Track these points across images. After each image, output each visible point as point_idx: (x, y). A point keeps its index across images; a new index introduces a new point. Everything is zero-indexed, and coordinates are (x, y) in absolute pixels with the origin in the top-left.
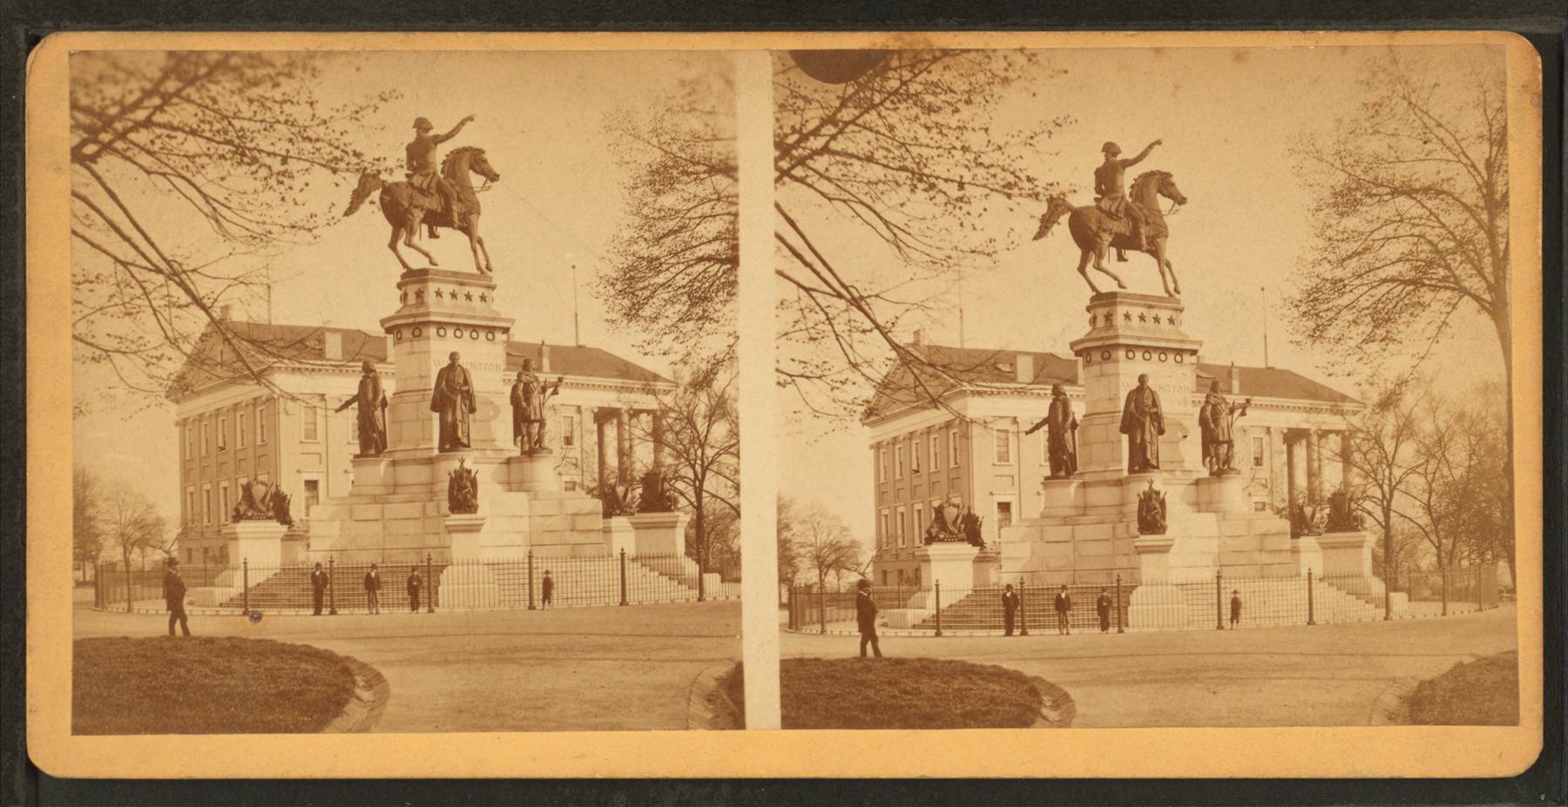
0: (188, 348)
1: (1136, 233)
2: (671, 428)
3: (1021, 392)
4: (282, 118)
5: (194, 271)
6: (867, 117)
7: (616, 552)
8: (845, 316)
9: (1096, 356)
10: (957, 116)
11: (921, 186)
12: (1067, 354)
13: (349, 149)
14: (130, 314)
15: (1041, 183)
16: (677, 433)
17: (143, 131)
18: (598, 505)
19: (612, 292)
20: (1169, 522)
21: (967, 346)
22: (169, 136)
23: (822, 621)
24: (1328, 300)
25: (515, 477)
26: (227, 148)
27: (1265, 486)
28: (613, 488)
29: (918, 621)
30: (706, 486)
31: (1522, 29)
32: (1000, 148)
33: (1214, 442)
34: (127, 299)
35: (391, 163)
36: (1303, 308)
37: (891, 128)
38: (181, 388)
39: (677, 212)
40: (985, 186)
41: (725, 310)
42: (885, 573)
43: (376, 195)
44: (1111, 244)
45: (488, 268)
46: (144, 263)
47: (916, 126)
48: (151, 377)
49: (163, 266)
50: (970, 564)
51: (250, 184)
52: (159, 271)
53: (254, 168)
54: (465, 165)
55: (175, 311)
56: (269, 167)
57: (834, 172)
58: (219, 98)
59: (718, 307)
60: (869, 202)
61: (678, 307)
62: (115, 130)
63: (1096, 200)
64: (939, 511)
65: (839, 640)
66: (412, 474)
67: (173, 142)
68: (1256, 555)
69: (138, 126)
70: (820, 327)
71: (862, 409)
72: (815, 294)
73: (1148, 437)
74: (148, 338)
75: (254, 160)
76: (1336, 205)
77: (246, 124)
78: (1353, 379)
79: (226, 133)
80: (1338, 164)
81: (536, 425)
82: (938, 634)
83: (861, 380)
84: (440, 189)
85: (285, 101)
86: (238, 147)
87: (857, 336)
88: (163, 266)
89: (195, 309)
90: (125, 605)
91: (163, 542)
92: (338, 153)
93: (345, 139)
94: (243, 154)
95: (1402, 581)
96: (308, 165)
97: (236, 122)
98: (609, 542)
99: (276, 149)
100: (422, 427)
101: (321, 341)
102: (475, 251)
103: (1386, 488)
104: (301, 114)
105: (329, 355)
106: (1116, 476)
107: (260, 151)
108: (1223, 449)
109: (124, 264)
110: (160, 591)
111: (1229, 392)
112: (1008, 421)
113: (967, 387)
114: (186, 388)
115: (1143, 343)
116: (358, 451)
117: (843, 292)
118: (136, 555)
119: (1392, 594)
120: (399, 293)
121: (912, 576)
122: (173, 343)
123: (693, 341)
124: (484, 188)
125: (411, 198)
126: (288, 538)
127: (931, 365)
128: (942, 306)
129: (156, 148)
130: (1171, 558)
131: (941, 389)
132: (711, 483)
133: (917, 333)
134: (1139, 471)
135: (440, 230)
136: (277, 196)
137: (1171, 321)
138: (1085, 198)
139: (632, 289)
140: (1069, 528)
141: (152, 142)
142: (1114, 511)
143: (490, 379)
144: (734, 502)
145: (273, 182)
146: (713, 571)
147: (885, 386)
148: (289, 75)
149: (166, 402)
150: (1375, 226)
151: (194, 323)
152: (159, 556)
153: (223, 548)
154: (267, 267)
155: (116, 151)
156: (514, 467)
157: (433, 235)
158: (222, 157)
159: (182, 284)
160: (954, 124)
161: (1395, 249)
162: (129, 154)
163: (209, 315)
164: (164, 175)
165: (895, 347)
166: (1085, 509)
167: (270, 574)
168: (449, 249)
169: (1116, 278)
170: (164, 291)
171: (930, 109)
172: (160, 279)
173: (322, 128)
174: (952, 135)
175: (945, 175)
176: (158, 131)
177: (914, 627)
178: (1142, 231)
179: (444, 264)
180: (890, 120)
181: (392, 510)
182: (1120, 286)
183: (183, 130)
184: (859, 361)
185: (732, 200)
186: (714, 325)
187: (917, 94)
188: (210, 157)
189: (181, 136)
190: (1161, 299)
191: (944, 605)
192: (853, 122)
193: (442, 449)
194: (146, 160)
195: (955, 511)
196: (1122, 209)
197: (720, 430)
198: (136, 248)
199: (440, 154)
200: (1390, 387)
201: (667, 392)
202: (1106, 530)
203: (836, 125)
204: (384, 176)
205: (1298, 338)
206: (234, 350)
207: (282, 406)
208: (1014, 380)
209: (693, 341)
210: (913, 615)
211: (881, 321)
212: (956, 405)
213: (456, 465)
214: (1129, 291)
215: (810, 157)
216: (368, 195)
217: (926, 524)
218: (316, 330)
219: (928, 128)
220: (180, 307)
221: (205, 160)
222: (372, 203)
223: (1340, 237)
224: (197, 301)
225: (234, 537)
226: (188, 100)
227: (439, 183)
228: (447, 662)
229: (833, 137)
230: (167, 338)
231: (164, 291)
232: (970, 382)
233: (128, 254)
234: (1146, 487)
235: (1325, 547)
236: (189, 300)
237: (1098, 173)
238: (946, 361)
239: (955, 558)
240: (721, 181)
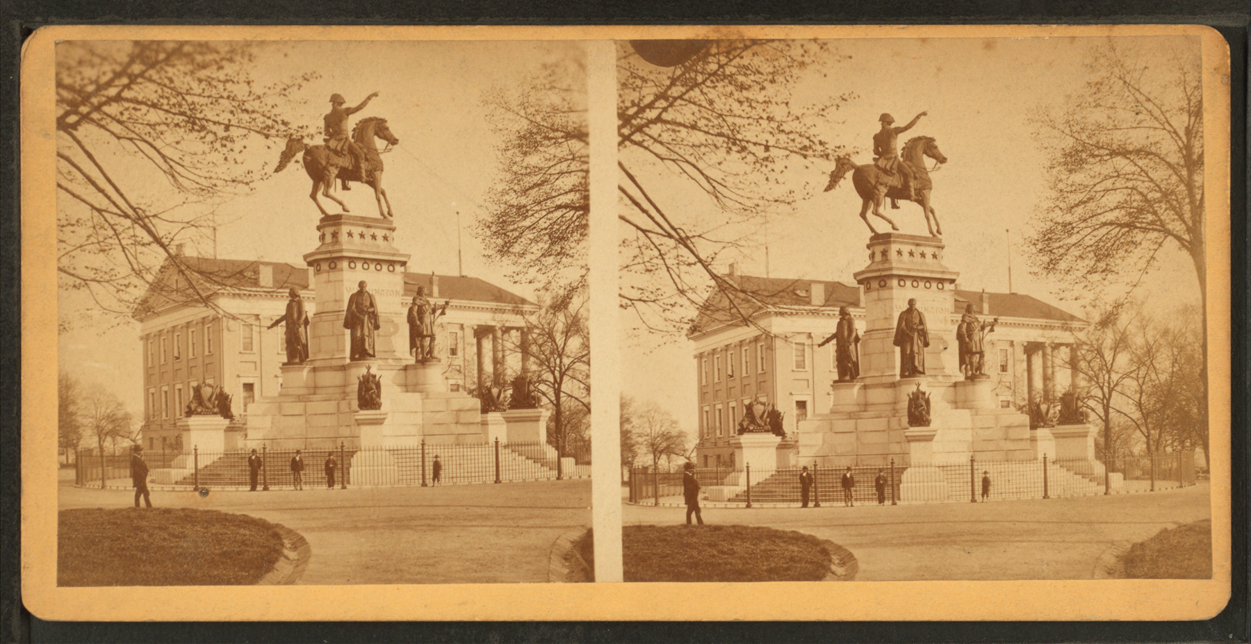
0: (150, 278)
1: (906, 186)
2: (535, 341)
3: (814, 313)
4: (225, 94)
5: (155, 216)
6: (692, 93)
7: (492, 441)
8: (674, 252)
10: (764, 92)
11: (735, 148)
12: (852, 282)
13: (279, 119)
14: (104, 251)
15: (831, 146)
16: (540, 346)
17: (114, 105)
18: (477, 403)
19: (489, 233)
20: (933, 416)
21: (772, 276)
22: (134, 109)
23: (656, 496)
24: (1059, 240)
25: (411, 381)
26: (181, 118)
28: (489, 390)
29: (732, 496)
30: (564, 387)
31: (1215, 23)
32: (798, 118)
33: (968, 353)
34: (101, 239)
35: (312, 130)
36: (1040, 246)
37: (711, 102)
38: (144, 310)
39: (540, 169)
40: (786, 149)
41: (579, 247)
42: (706, 457)
43: (300, 156)
44: (338, 176)
46: (115, 210)
47: (731, 100)
48: (121, 301)
49: (130, 212)
50: (774, 450)
51: (200, 147)
52: (127, 216)
53: (202, 134)
54: (371, 131)
55: (139, 248)
56: (215, 134)
57: (666, 137)
58: (175, 78)
59: (573, 245)
60: (694, 161)
61: (541, 245)
62: (92, 104)
63: (875, 159)
64: (749, 408)
65: (669, 511)
66: (329, 379)
67: (138, 113)
69: (110, 100)
70: (655, 261)
73: (366, 332)
74: (118, 269)
75: (203, 128)
77: (196, 99)
79: (180, 106)
80: (1067, 131)
81: (428, 339)
82: (748, 506)
83: (687, 303)
84: (351, 151)
85: (227, 81)
86: (189, 117)
87: (684, 268)
88: (130, 212)
89: (155, 247)
90: (100, 483)
91: (131, 433)
92: (270, 122)
93: (275, 111)
94: (194, 123)
95: (1118, 464)
96: (246, 132)
97: (188, 97)
98: (486, 433)
99: (220, 119)
100: (337, 341)
101: (256, 272)
102: (379, 201)
103: (1106, 390)
104: (240, 91)
105: (262, 284)
107: (207, 121)
108: (976, 358)
109: (99, 211)
110: (128, 472)
111: (981, 313)
112: (805, 336)
113: (771, 309)
114: (149, 309)
115: (912, 274)
116: (285, 360)
117: (673, 233)
118: (108, 443)
120: (318, 234)
122: (138, 274)
123: (553, 273)
124: (386, 150)
125: (328, 158)
126: (230, 429)
129: (124, 118)
132: (567, 386)
133: (731, 266)
134: (909, 376)
135: (351, 184)
137: (934, 256)
138: (865, 158)
139: (504, 230)
140: (853, 421)
141: (122, 114)
142: (889, 407)
143: (391, 302)
144: (585, 401)
145: (218, 145)
146: (569, 456)
147: (706, 308)
148: (231, 60)
149: (132, 320)
150: (1097, 180)
151: (155, 258)
152: (127, 443)
153: (178, 437)
155: (93, 120)
156: (960, 389)
157: (345, 188)
158: (177, 125)
159: (145, 227)
160: (761, 99)
161: (1113, 199)
162: (103, 123)
163: (167, 251)
164: (131, 139)
165: (714, 277)
166: (866, 406)
167: (216, 458)
168: (358, 199)
169: (890, 222)
170: (131, 232)
171: (742, 87)
172: (128, 222)
173: (257, 102)
174: (760, 108)
175: (754, 140)
176: (126, 105)
177: (729, 500)
178: (911, 184)
179: (355, 211)
180: (710, 96)
183: (146, 104)
184: (686, 288)
185: (584, 159)
186: (570, 260)
187: (731, 75)
188: (168, 125)
189: (144, 108)
190: (926, 239)
191: (753, 483)
192: (680, 97)
193: (352, 358)
194: (116, 128)
195: (762, 407)
196: (895, 166)
197: (574, 343)
198: (108, 198)
199: (351, 123)
200: (1109, 308)
201: (532, 313)
202: (882, 424)
203: (667, 100)
204: (306, 141)
205: (1035, 269)
206: (187, 279)
207: (225, 324)
208: (809, 303)
209: (553, 273)
210: (728, 491)
211: (703, 257)
212: (763, 323)
213: (364, 371)
214: (901, 232)
215: (647, 125)
216: (294, 156)
217: (739, 418)
218: (252, 263)
219: (741, 102)
220: (143, 245)
221: (163, 128)
222: (297, 162)
223: (1069, 189)
224: (158, 240)
225: (187, 429)
226: (150, 80)
227: (350, 145)
228: (356, 528)
229: (665, 110)
230: (133, 269)
231: (131, 232)
232: (774, 305)
233: (102, 202)
234: (914, 388)
235: (1057, 436)
236: (151, 239)
237: (876, 138)
238: (755, 288)
240: (576, 145)
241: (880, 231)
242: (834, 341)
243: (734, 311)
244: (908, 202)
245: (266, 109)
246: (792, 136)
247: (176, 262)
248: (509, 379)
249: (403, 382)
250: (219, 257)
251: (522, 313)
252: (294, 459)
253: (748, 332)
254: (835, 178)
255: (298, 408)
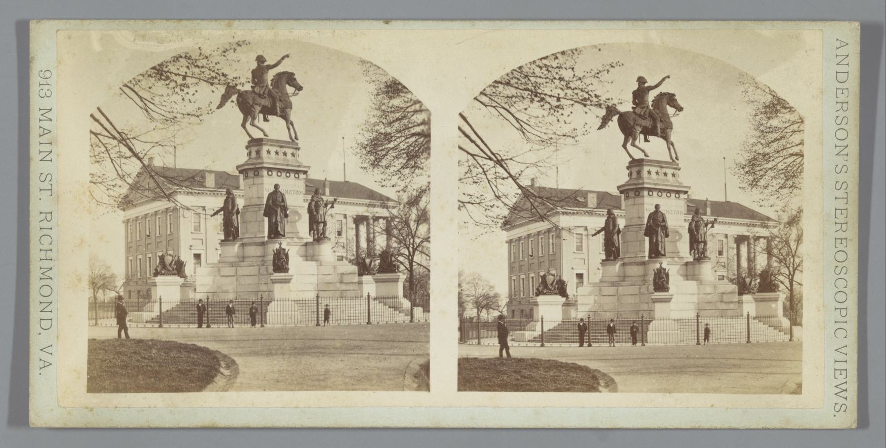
0: (130, 181)
2: (396, 227)
3: (590, 213)
5: (134, 138)
7: (365, 295)
8: (493, 170)
9: (251, 174)
10: (557, 61)
11: (536, 99)
13: (220, 72)
15: (603, 98)
18: (355, 269)
20: (291, 265)
21: (560, 187)
23: (479, 338)
24: (760, 165)
27: (724, 267)
28: (364, 260)
32: (580, 79)
35: (243, 80)
36: (747, 169)
39: (401, 108)
40: (572, 100)
43: (234, 98)
45: (677, 158)
46: (106, 133)
49: (117, 135)
53: (167, 82)
54: (284, 82)
55: (123, 160)
60: (507, 107)
61: (401, 160)
65: (488, 348)
68: (338, 285)
70: (479, 176)
71: (502, 221)
72: (477, 158)
73: (660, 239)
75: (168, 78)
76: (765, 113)
78: (773, 209)
83: (502, 205)
84: (270, 94)
86: (158, 70)
88: (117, 135)
89: (134, 159)
90: (94, 322)
93: (218, 67)
101: (203, 177)
103: (791, 269)
106: (261, 240)
107: (171, 73)
110: (113, 314)
111: (705, 214)
113: (559, 210)
116: (604, 258)
117: (492, 157)
119: (794, 327)
121: (528, 312)
122: (122, 178)
123: (408, 180)
124: (294, 94)
125: (254, 100)
126: (183, 286)
127: (541, 198)
128: (547, 165)
130: (672, 305)
131: (545, 211)
133: (533, 180)
134: (274, 238)
136: (180, 98)
138: (627, 106)
139: (376, 149)
145: (177, 90)
147: (514, 209)
153: (149, 291)
154: (174, 136)
163: (142, 162)
165: (520, 187)
166: (243, 258)
170: (117, 149)
172: (115, 142)
174: (554, 71)
177: (529, 341)
179: (272, 136)
181: (243, 271)
182: (646, 155)
184: (501, 194)
186: (421, 171)
196: (647, 113)
198: (102, 125)
200: (794, 213)
201: (394, 207)
204: (239, 87)
206: (155, 182)
208: (586, 206)
209: (408, 180)
210: (528, 335)
211: (513, 173)
214: (269, 138)
216: (230, 97)
217: (536, 285)
218: (201, 171)
219: (541, 68)
220: (126, 158)
224: (136, 155)
230: (118, 174)
231: (117, 149)
232: (561, 207)
239: (551, 304)
241: (636, 157)
242: (603, 233)
243: (534, 211)
244: (275, 117)
245: (211, 65)
246: (576, 91)
247: (148, 170)
248: (378, 252)
249: (303, 253)
250: (177, 167)
251: (387, 207)
252: (228, 306)
253: (543, 226)
254: (605, 121)
255: (612, 290)
